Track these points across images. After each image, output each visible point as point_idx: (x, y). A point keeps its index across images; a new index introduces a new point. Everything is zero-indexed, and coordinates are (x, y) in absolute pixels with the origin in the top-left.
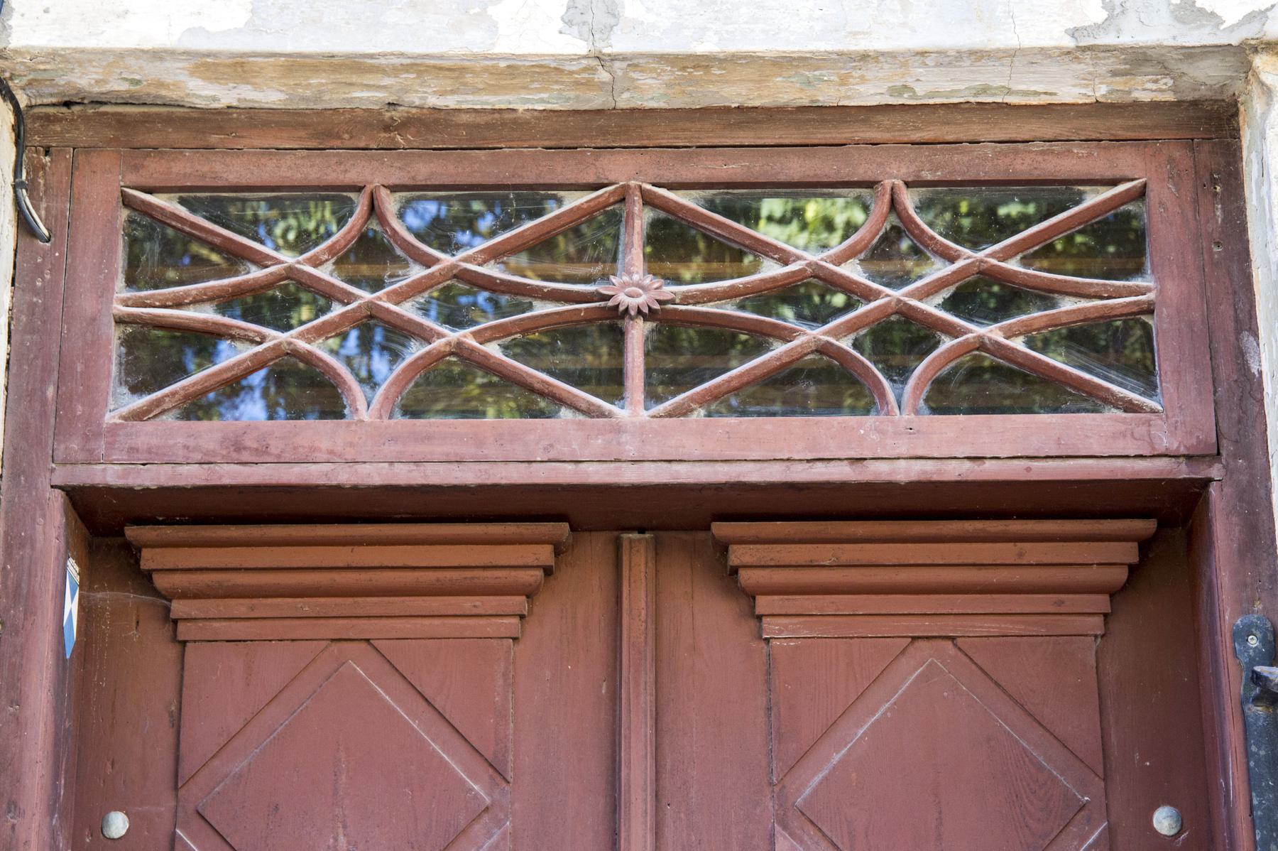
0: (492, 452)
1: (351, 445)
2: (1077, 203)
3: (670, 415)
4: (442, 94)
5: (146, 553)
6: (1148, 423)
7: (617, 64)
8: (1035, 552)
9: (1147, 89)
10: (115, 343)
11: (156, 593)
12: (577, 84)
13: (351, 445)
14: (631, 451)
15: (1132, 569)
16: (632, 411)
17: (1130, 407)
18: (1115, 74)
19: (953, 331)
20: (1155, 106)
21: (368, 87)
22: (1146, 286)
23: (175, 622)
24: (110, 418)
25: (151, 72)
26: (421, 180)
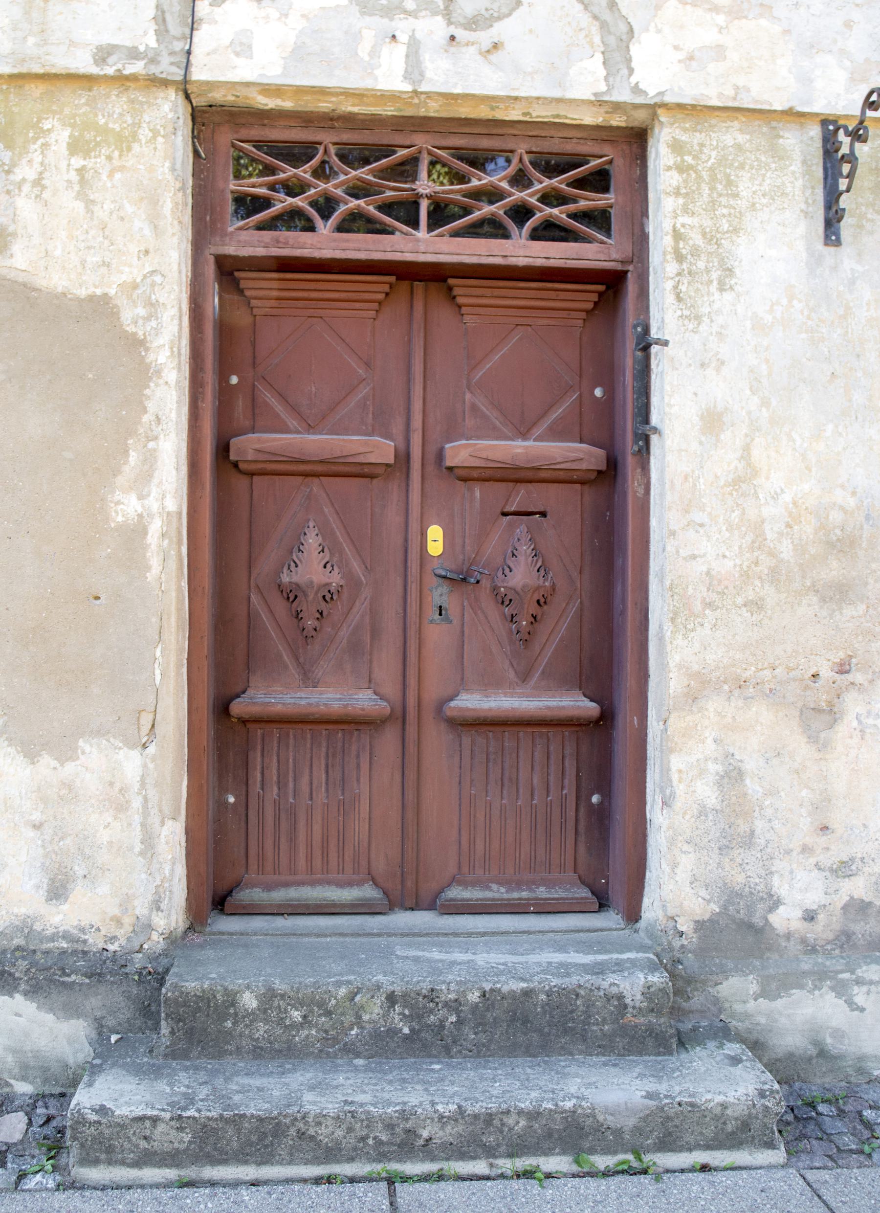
0: (371, 247)
1: (319, 242)
2: (587, 164)
3: (437, 236)
4: (353, 105)
5: (242, 282)
6: (609, 248)
7: (423, 96)
8: (562, 295)
9: (618, 121)
10: (230, 200)
11: (245, 296)
12: (406, 103)
13: (319, 242)
14: (422, 248)
15: (596, 303)
16: (422, 233)
17: (602, 242)
18: (607, 113)
19: (541, 211)
20: (618, 128)
21: (326, 102)
22: (610, 198)
23: (252, 308)
24: (231, 229)
25: (243, 92)
26: (344, 141)
